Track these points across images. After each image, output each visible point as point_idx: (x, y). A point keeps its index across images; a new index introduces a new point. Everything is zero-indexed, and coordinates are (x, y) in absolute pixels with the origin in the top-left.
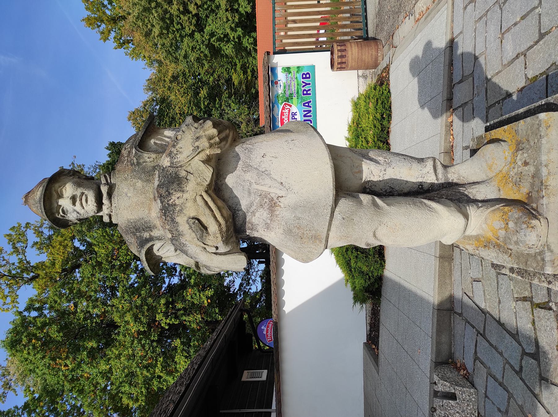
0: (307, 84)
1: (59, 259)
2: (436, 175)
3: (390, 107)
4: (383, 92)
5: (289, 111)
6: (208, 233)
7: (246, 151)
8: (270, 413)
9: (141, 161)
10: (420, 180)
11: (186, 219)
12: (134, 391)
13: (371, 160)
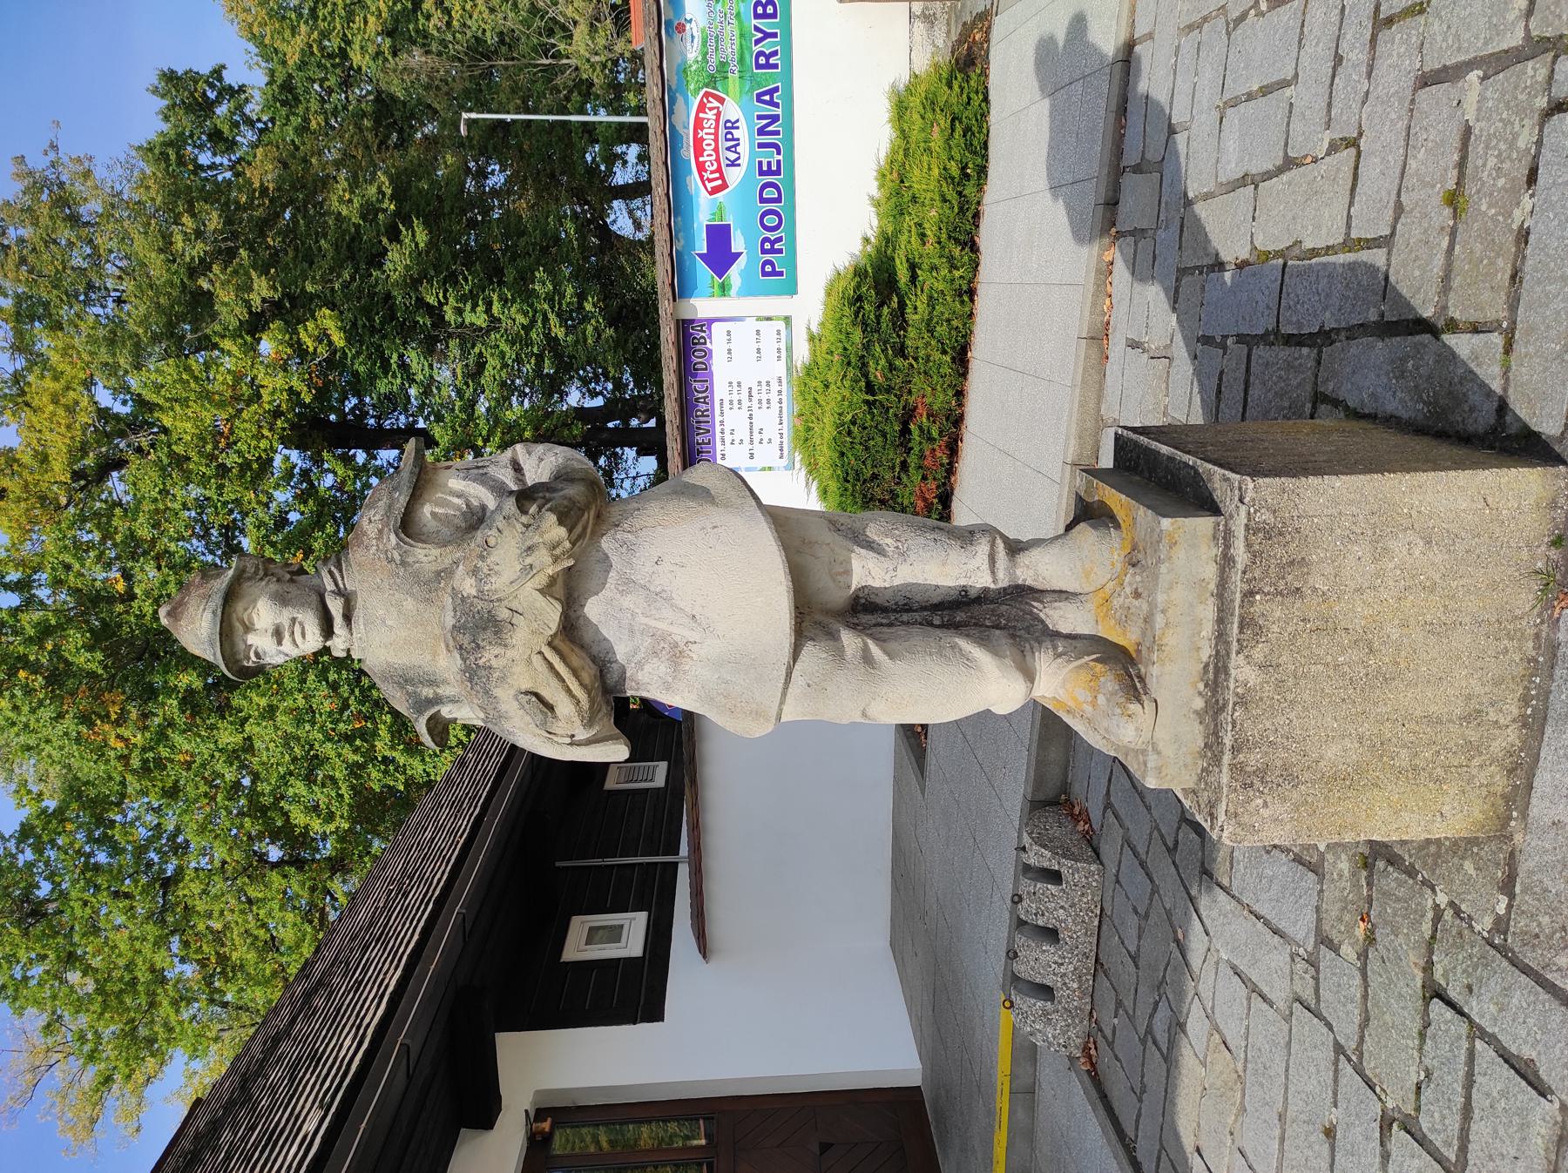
0: (767, 35)
1: (58, 447)
2: (993, 572)
3: (985, 146)
4: (969, 99)
5: (718, 115)
6: (555, 717)
7: (624, 550)
8: (676, 864)
9: (411, 560)
10: (963, 582)
11: (512, 692)
12: (321, 796)
13: (870, 545)
